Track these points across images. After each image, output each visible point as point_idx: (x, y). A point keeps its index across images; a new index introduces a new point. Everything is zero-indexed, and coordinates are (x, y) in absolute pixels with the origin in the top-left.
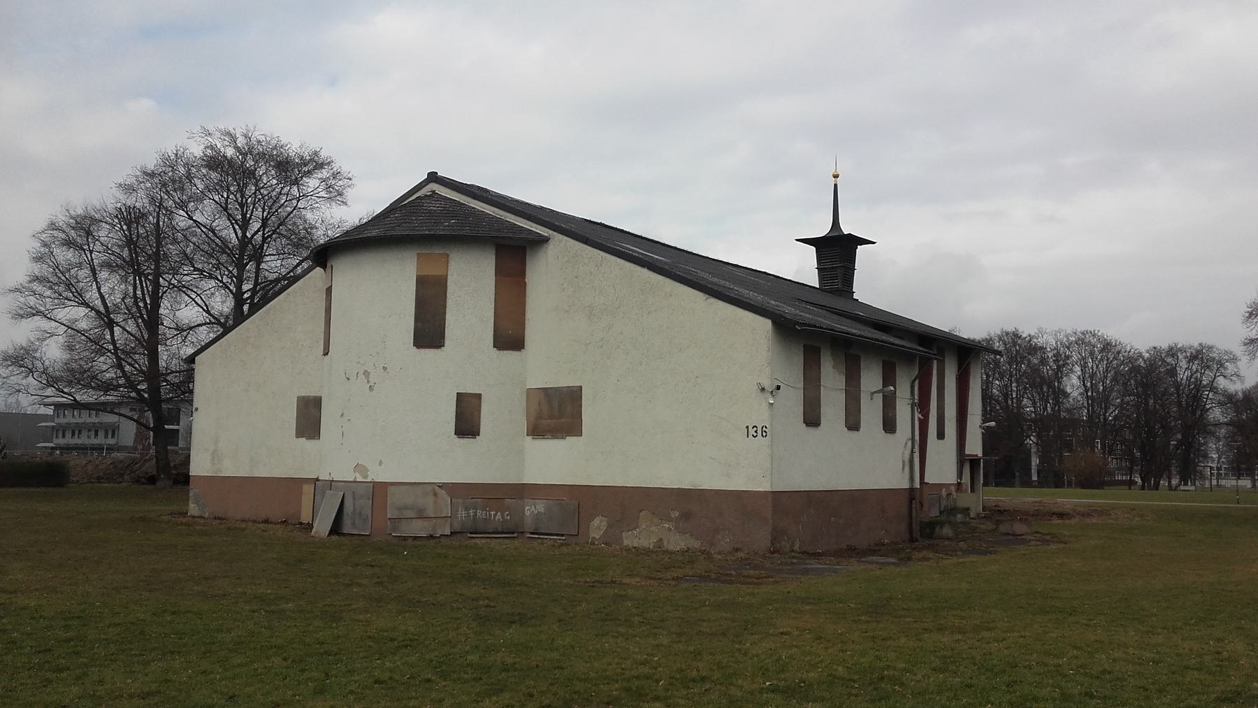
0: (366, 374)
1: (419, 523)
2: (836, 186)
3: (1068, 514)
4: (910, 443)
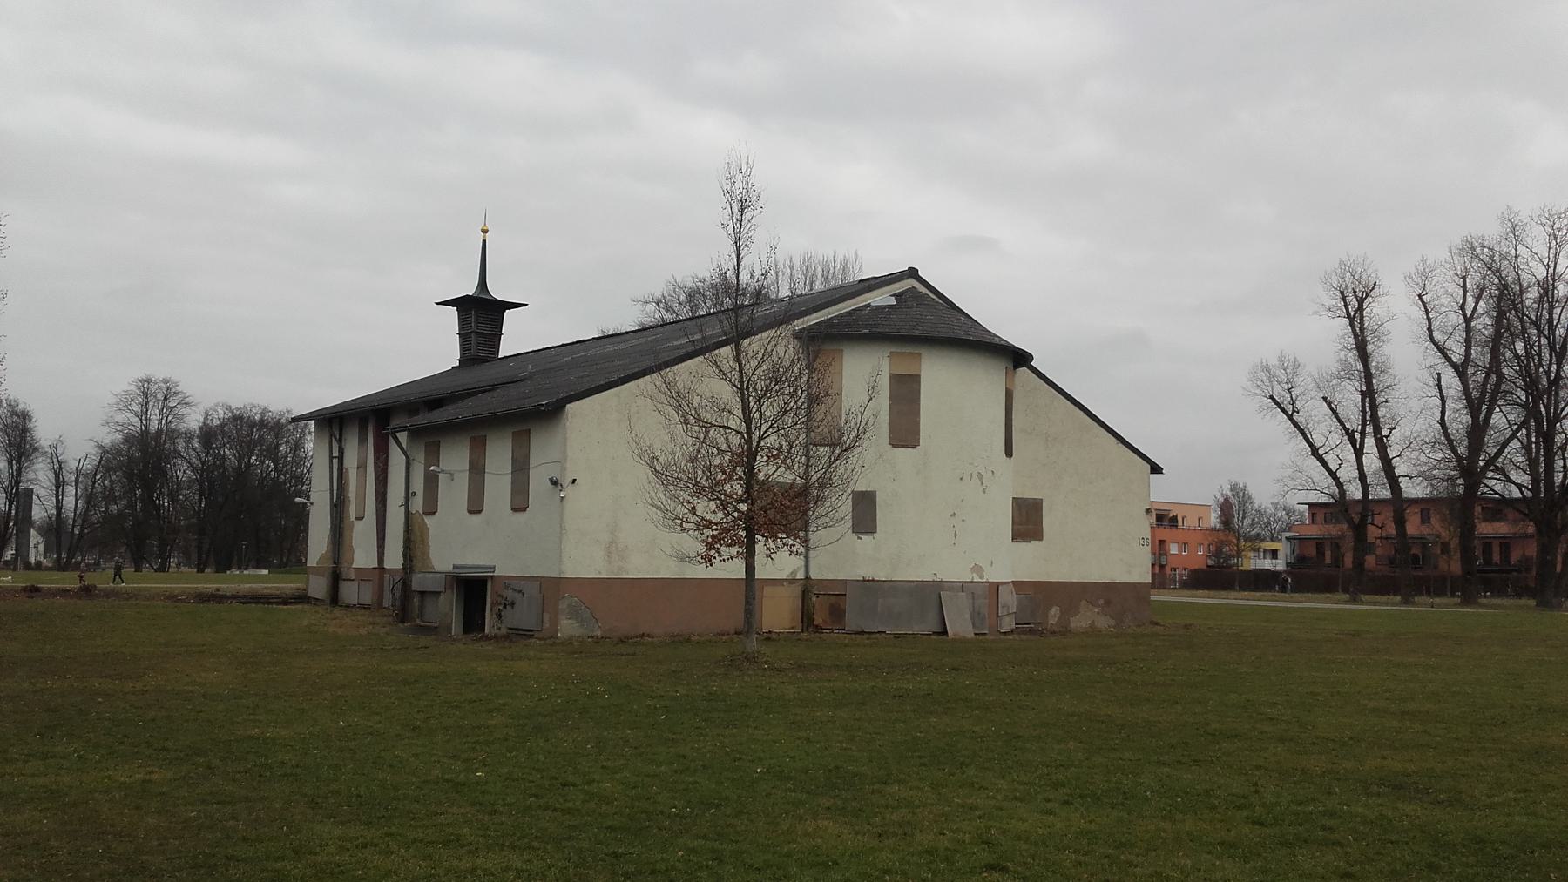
0: (980, 476)
2: (484, 242)
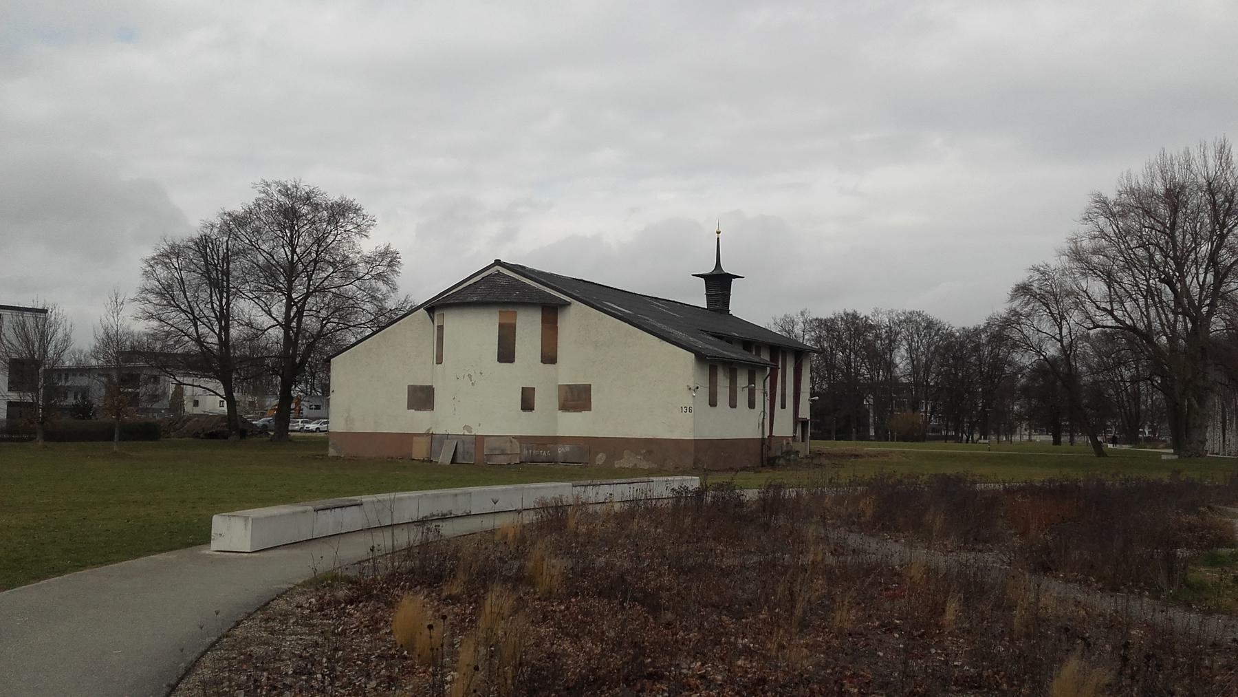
0: (470, 376)
1: (502, 457)
2: (718, 239)
3: (861, 455)
4: (762, 414)
